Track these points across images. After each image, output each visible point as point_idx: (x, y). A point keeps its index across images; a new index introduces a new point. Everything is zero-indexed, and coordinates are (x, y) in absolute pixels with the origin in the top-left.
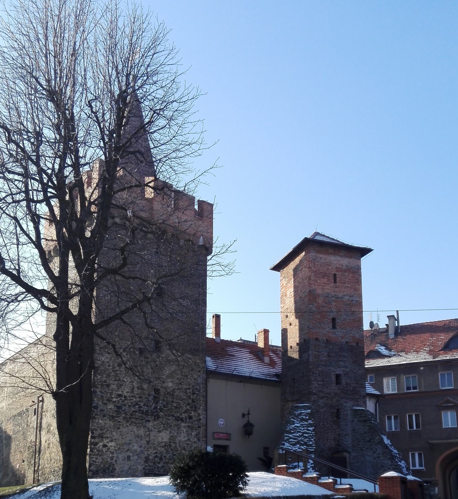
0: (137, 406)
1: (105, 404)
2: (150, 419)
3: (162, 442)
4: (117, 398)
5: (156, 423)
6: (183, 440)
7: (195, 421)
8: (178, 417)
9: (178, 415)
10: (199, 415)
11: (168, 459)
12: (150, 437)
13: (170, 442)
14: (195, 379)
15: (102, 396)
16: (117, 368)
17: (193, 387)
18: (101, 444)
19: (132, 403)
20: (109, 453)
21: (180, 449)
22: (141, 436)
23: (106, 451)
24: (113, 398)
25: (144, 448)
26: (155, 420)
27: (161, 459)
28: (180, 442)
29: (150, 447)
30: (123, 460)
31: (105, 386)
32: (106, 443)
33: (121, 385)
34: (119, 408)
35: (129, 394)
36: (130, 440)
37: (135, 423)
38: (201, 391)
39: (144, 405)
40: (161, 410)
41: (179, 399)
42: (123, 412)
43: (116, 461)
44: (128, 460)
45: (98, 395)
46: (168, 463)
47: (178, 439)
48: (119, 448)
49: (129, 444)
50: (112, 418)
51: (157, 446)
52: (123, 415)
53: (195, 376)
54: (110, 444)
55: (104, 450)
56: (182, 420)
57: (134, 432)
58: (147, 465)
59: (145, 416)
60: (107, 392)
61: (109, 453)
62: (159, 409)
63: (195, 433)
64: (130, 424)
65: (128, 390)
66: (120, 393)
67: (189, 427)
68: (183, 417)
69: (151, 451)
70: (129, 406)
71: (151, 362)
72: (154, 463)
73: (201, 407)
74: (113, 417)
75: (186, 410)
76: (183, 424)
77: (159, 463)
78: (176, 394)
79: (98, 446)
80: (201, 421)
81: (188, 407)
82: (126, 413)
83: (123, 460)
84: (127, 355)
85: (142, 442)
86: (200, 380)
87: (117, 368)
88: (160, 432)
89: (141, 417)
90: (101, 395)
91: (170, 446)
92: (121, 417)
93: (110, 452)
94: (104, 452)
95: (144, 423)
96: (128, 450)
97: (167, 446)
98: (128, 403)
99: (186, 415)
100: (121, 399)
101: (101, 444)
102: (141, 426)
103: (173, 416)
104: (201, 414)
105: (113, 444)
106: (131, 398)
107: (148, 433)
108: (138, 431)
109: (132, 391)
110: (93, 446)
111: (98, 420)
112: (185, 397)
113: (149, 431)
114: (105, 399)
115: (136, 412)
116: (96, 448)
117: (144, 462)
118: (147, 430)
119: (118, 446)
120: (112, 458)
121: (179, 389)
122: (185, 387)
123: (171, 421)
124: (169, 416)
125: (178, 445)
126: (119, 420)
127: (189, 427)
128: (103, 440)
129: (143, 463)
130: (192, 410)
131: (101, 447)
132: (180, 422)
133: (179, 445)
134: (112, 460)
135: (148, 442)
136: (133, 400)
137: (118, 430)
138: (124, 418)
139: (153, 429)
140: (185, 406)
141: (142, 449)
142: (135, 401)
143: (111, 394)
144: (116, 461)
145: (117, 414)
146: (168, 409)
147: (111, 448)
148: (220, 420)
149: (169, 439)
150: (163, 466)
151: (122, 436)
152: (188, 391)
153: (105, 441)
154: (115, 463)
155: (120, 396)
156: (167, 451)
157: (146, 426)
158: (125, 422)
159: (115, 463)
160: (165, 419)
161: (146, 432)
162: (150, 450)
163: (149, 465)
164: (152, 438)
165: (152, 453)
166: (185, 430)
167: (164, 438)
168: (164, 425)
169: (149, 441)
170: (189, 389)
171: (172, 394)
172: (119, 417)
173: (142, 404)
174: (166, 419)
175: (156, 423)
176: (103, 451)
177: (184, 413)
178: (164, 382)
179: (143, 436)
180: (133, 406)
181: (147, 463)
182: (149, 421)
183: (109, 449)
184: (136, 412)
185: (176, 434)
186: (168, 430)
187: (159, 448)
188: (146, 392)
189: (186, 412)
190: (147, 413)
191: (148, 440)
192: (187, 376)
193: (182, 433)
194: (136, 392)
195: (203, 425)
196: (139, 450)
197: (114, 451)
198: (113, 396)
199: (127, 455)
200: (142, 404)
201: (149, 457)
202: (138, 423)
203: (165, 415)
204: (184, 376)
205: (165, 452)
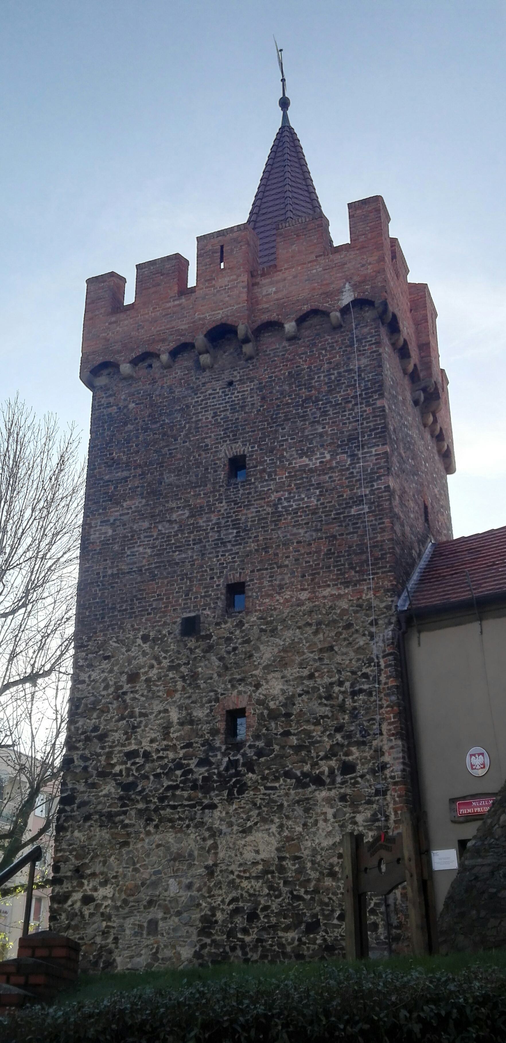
0: (179, 773)
1: (94, 786)
2: (216, 801)
3: (255, 863)
4: (126, 763)
5: (235, 806)
6: (325, 844)
7: (362, 776)
8: (305, 775)
9: (307, 768)
10: (379, 752)
11: (277, 915)
12: (216, 854)
13: (281, 859)
14: (360, 650)
15: (85, 768)
16: (126, 687)
17: (353, 673)
18: (77, 896)
19: (163, 767)
20: (97, 918)
21: (314, 875)
22: (191, 855)
23: (91, 915)
24: (113, 766)
25: (199, 890)
26: (230, 799)
27: (252, 916)
28: (315, 852)
29: (219, 885)
30: (136, 934)
31: (95, 740)
32: (89, 893)
33: (134, 727)
34: (127, 787)
35: (155, 745)
36: (155, 873)
37: (171, 820)
38: (383, 678)
39: (198, 765)
40: (250, 766)
41: (308, 722)
42: (139, 798)
43: (116, 940)
44: (149, 934)
45: (75, 767)
46: (274, 927)
47: (309, 844)
48: (125, 902)
49: (155, 885)
50: (109, 819)
51: (239, 876)
52: (141, 806)
53: (361, 642)
54: (102, 892)
55: (86, 913)
56: (318, 781)
57: (168, 849)
58: (208, 941)
59: (200, 795)
60: (99, 755)
61: (97, 918)
62: (244, 765)
63: (369, 814)
64: (156, 827)
65: (153, 736)
66: (134, 747)
67: (343, 798)
68: (322, 773)
69: (223, 896)
70: (157, 776)
71: (218, 644)
72: (231, 934)
73: (385, 727)
74: (110, 816)
75: (332, 746)
76: (323, 794)
77: (245, 931)
78: (295, 710)
79: (69, 903)
80: (387, 772)
81: (339, 737)
82: (146, 799)
83: (136, 934)
84: (152, 648)
85: (193, 871)
86: (377, 648)
87: (126, 687)
88: (246, 831)
89: (189, 799)
90: (82, 764)
91: (282, 869)
92: (133, 813)
93: (102, 914)
94: (87, 917)
95: (198, 816)
96: (151, 903)
97: (269, 871)
98: (154, 770)
99: (333, 763)
100: (134, 764)
101: (77, 896)
102: (188, 826)
103: (288, 775)
104: (386, 748)
105: (107, 891)
106: (161, 754)
107: (210, 842)
108: (179, 841)
109: (166, 735)
110: (56, 906)
111: (72, 832)
112: (325, 710)
113: (213, 836)
114: (95, 772)
115: (176, 787)
116: (65, 911)
117: (199, 935)
118: (207, 834)
119: (124, 896)
120: (105, 934)
121: (307, 692)
122: (327, 680)
123: (285, 792)
124: (277, 779)
125: (309, 865)
126: (127, 821)
127: (343, 798)
128: (81, 885)
129: (195, 938)
130: (349, 745)
131: (78, 904)
132: (313, 787)
133: (313, 862)
134: (106, 938)
135: (211, 871)
136: (167, 757)
137: (124, 851)
138: (140, 813)
139: (224, 828)
140: (330, 736)
141: (195, 893)
142: (173, 760)
143: (109, 756)
144: (116, 940)
145: (123, 805)
146: (272, 759)
147: (105, 903)
148: (472, 751)
149: (278, 849)
150: (259, 940)
151: (134, 864)
152: (336, 689)
153: (88, 886)
154: (113, 946)
155: (131, 755)
156: (271, 888)
157: (202, 824)
158: (142, 822)
159: (113, 946)
160: (263, 791)
161: (204, 839)
162: (217, 892)
163: (213, 941)
164: (221, 855)
165: (223, 901)
166: (330, 812)
167: (261, 847)
168: (260, 808)
169: (215, 865)
170: (341, 684)
171: (282, 714)
172: (125, 813)
173: (193, 763)
174: (267, 788)
175: (235, 806)
176: (83, 916)
177: (326, 758)
178: (258, 686)
179: (196, 853)
180: (166, 774)
181: (209, 935)
182: (213, 807)
183: (98, 906)
184: (176, 787)
185: (299, 829)
186: (272, 821)
187: (245, 884)
188: (206, 727)
189: (331, 754)
190: (206, 786)
191: (210, 862)
192: (331, 648)
193: (321, 824)
194: (176, 735)
195: (395, 784)
196: (185, 895)
197: (113, 912)
198: (114, 761)
199: (150, 917)
200: (193, 763)
201: (214, 915)
202: (180, 819)
203: (264, 778)
204: (321, 651)
205: (266, 891)
